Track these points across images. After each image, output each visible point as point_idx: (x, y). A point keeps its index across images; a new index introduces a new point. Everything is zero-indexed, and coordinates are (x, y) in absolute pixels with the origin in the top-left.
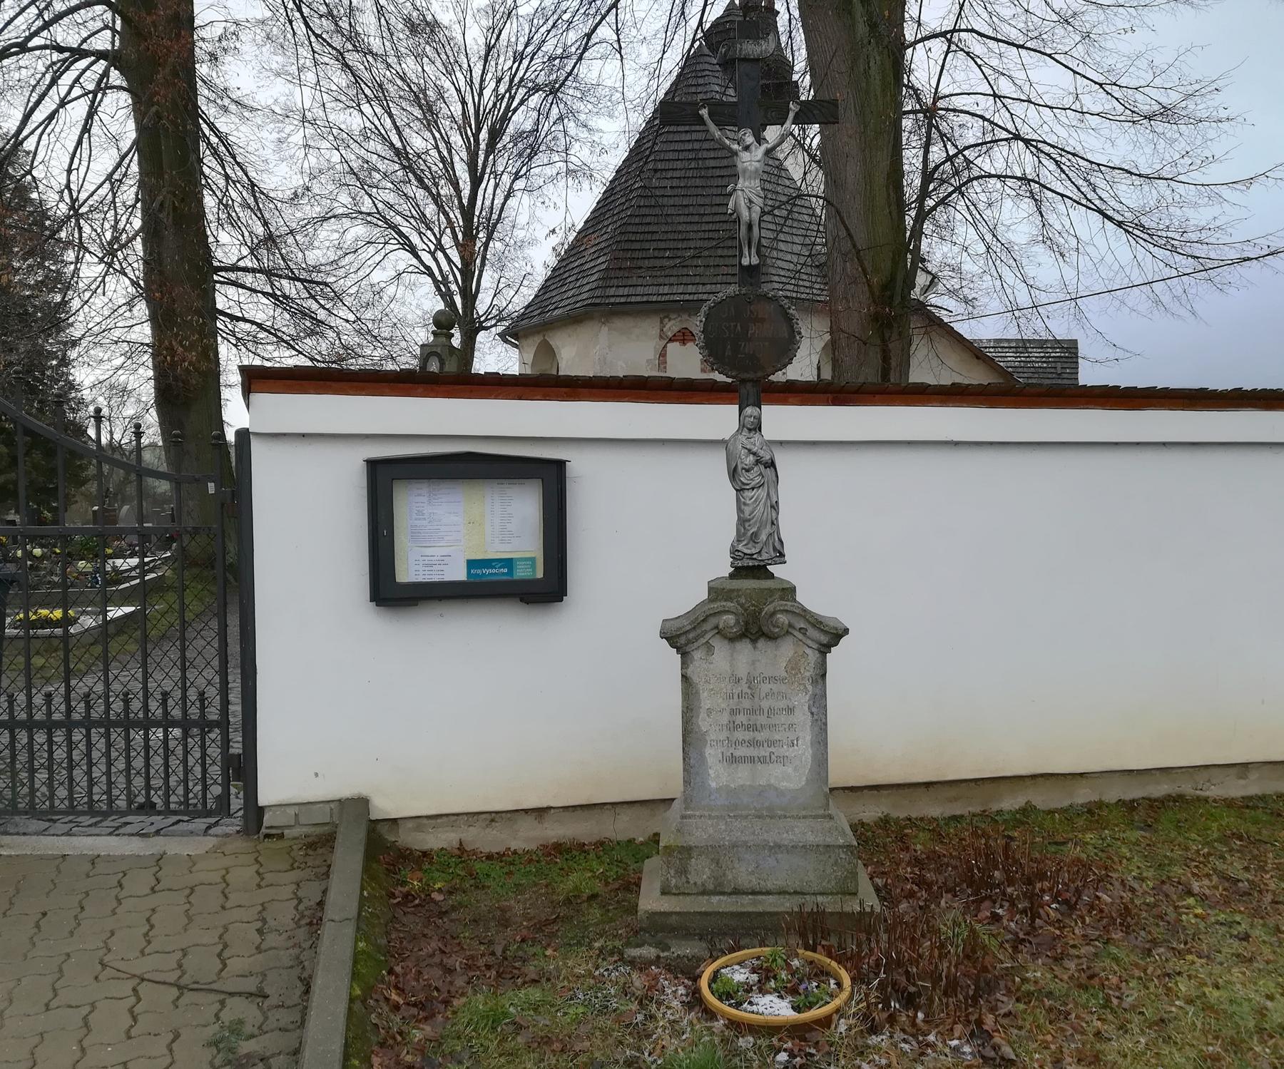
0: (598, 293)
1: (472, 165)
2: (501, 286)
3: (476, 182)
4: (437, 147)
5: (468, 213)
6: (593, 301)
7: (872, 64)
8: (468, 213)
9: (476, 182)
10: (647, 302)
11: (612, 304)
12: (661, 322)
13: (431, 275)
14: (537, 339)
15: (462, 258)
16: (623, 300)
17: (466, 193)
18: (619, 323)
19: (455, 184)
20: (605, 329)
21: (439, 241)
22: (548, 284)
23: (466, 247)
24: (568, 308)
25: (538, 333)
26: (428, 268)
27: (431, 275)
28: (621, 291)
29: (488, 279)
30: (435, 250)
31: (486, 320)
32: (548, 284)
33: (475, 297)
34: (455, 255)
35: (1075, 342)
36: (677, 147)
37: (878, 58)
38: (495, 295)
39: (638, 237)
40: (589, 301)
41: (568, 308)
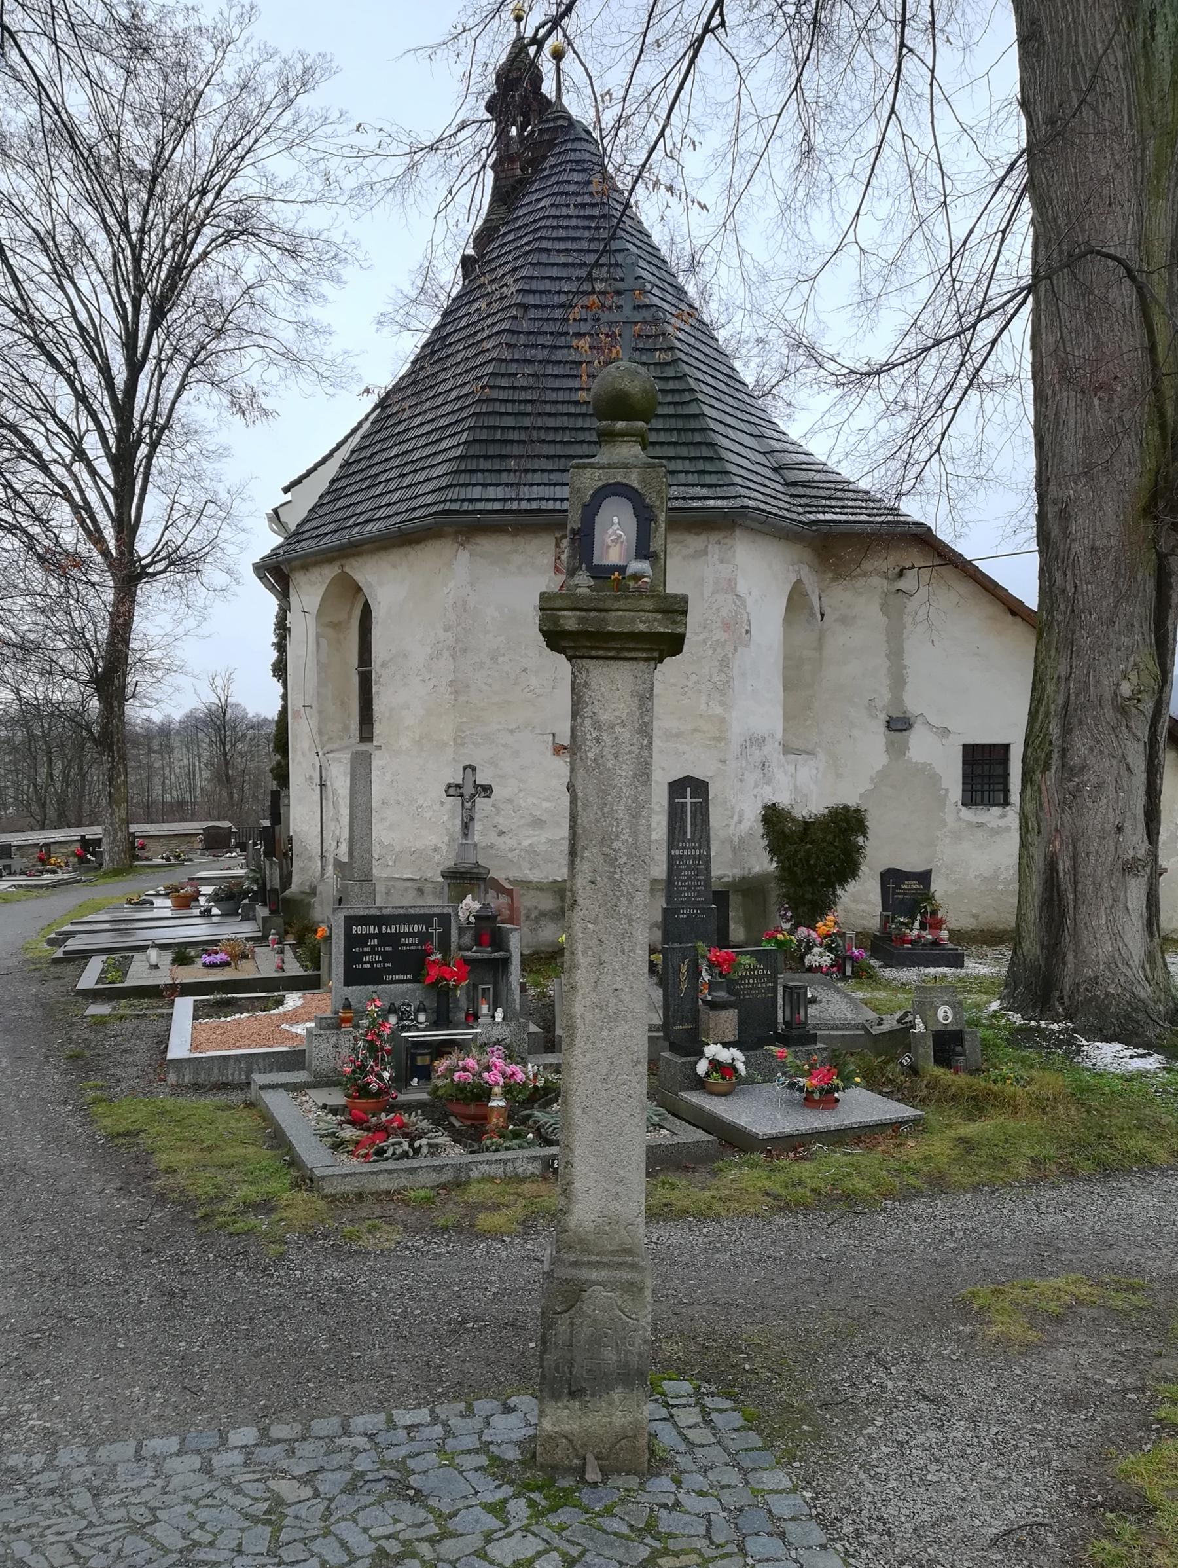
0: (453, 494)
1: (129, 342)
2: (176, 515)
3: (135, 367)
4: (74, 313)
5: (123, 411)
6: (447, 506)
7: (1158, 29)
8: (123, 411)
9: (135, 367)
10: (539, 511)
11: (480, 512)
12: (557, 545)
13: (68, 497)
14: (329, 572)
15: (116, 472)
16: (497, 506)
17: (120, 378)
18: (487, 545)
19: (105, 370)
20: (464, 555)
21: (167, 338)
22: (337, 485)
23: (122, 461)
24: (398, 519)
25: (330, 561)
26: (62, 486)
27: (68, 497)
28: (491, 492)
29: (153, 506)
30: (73, 461)
31: (152, 563)
32: (337, 485)
33: (134, 529)
34: (105, 469)
35: (684, 599)
36: (555, 272)
37: (1170, 19)
38: (166, 528)
39: (509, 408)
40: (441, 507)
41: (398, 519)
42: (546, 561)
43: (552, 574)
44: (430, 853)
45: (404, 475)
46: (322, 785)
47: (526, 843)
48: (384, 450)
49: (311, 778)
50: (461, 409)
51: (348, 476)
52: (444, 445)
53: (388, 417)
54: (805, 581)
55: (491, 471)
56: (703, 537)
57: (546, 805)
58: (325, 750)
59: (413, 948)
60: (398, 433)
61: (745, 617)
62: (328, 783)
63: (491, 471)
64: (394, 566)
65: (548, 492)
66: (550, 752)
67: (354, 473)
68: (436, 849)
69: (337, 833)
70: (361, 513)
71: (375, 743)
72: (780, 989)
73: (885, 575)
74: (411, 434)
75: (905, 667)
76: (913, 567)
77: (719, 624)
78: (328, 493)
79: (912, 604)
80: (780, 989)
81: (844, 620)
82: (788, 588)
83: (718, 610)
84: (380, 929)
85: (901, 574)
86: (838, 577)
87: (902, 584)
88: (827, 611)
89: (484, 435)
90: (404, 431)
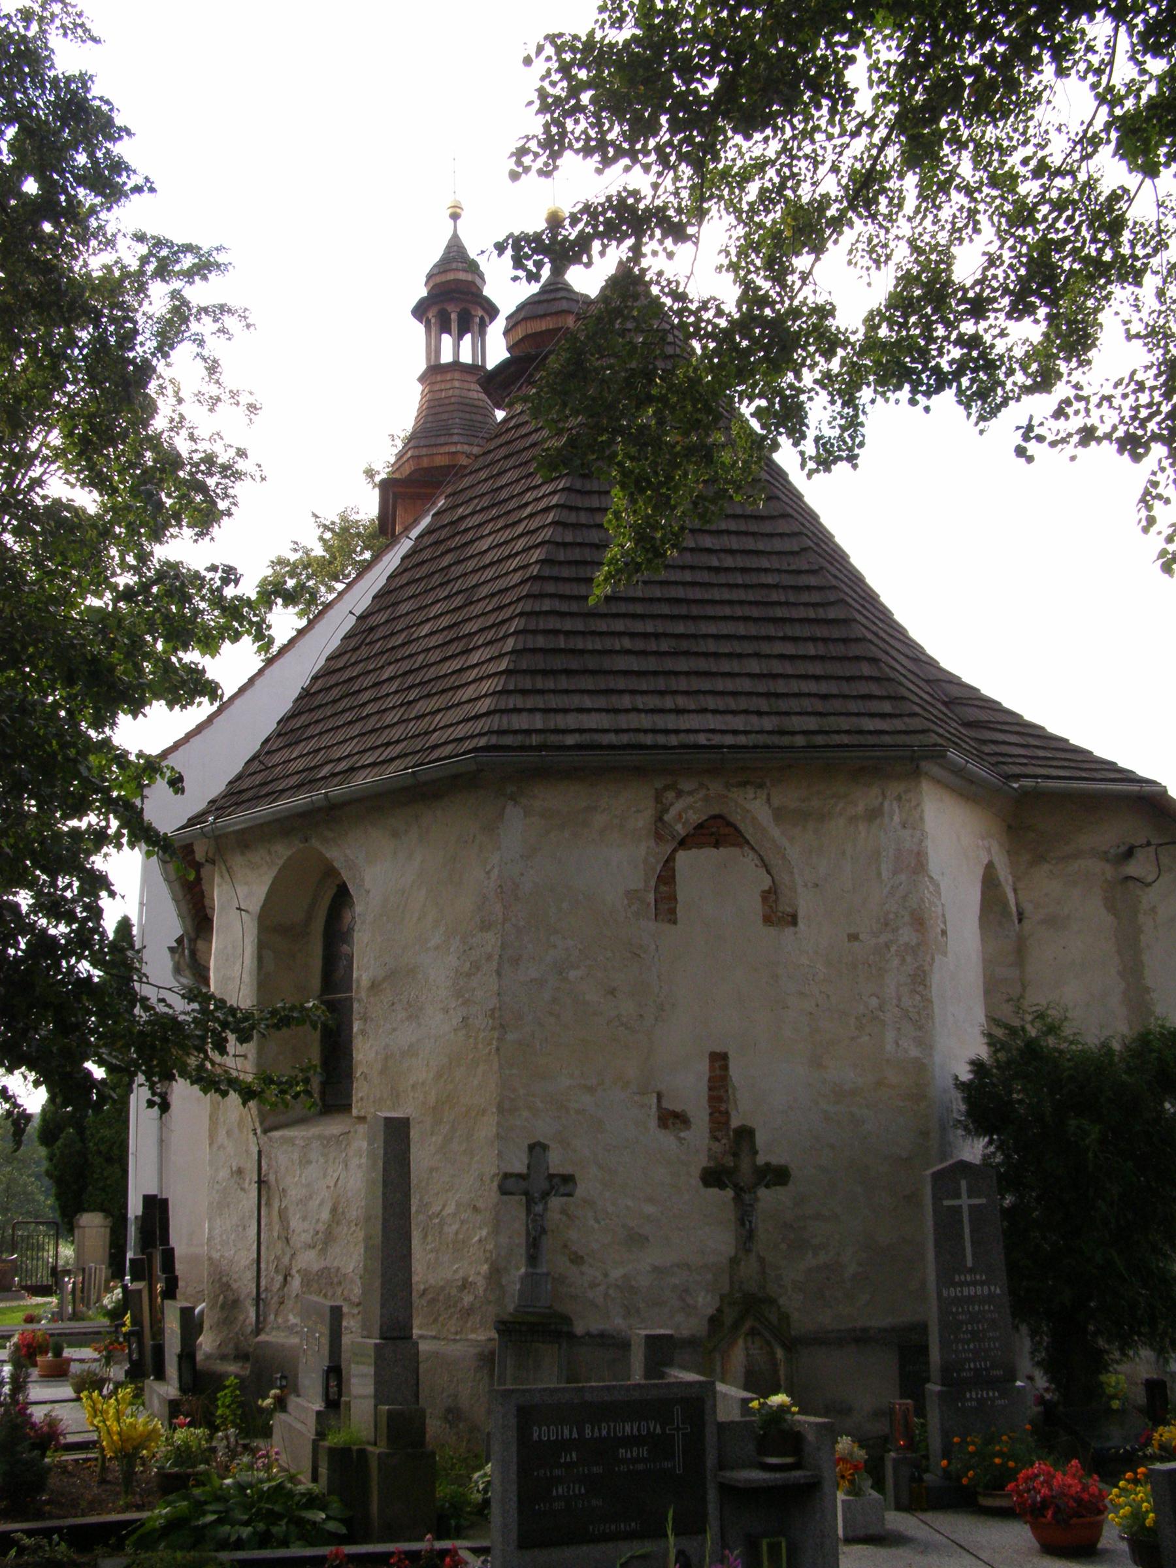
20: (513, 813)
42: (640, 824)
43: (652, 843)
44: (454, 1292)
45: (410, 703)
46: (260, 1182)
47: (616, 1274)
48: (370, 672)
49: (240, 1171)
50: (500, 608)
51: (311, 710)
52: (475, 658)
53: (372, 629)
54: (998, 865)
55: (554, 692)
56: (875, 791)
57: (649, 1209)
58: (266, 1124)
59: (640, 1467)
60: (393, 648)
61: (939, 910)
62: (272, 1178)
63: (554, 692)
64: (395, 834)
65: (646, 721)
66: (653, 1123)
67: (319, 707)
68: (465, 1285)
69: (286, 1260)
70: (340, 759)
71: (355, 1112)
72: (712, 1495)
73: (1105, 857)
74: (412, 649)
75: (1147, 990)
76: (1149, 844)
77: (907, 918)
78: (279, 735)
79: (1149, 897)
80: (712, 1495)
81: (1053, 922)
82: (980, 872)
83: (905, 897)
84: (581, 1432)
85: (1129, 853)
86: (1039, 859)
87: (1132, 869)
88: (1028, 908)
89: (540, 642)
90: (403, 645)
